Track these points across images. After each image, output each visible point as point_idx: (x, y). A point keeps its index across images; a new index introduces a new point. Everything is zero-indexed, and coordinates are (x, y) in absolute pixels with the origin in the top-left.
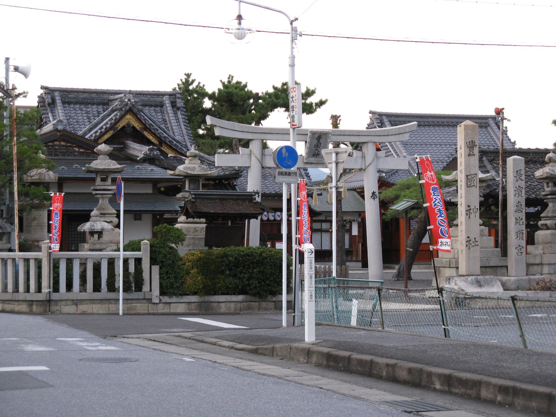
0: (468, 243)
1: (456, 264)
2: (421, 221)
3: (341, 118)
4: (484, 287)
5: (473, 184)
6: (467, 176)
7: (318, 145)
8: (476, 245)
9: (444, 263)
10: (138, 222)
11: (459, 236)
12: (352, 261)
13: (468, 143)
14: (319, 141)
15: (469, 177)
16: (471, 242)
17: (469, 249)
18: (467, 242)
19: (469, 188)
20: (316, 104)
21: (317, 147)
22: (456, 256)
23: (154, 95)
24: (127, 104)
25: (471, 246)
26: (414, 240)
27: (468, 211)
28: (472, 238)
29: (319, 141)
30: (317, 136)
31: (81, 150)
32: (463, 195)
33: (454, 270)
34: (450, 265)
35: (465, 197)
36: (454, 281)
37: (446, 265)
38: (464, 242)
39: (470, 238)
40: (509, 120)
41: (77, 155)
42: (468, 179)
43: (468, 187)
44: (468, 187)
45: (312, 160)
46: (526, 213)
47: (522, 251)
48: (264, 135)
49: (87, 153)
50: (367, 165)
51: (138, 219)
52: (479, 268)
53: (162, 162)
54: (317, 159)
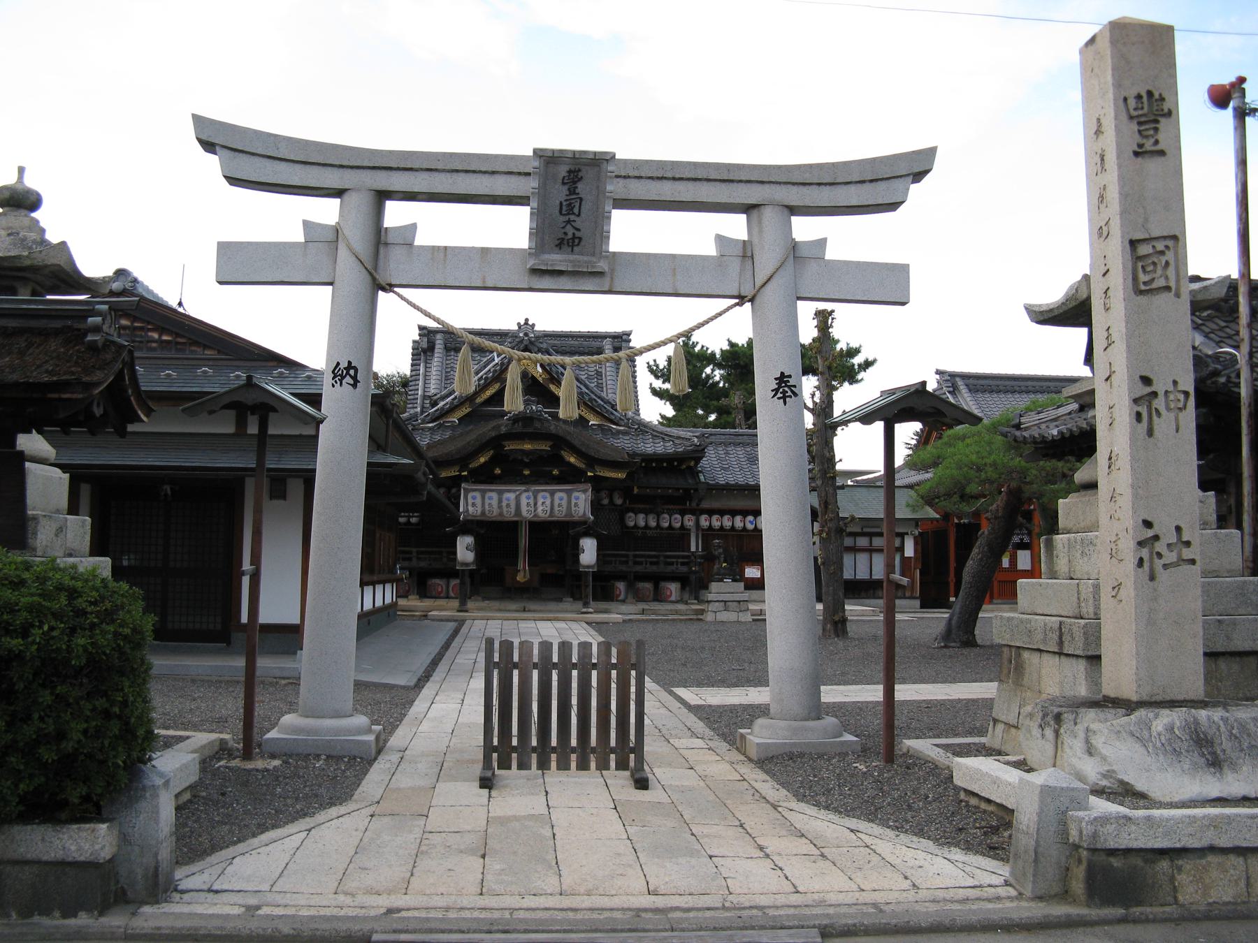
0: (1145, 553)
1: (1087, 644)
2: (996, 518)
3: (835, 315)
4: (1234, 767)
5: (1161, 283)
6: (1133, 244)
7: (570, 207)
8: (1182, 561)
9: (1039, 636)
11: (1104, 520)
12: (905, 597)
13: (1132, 103)
14: (572, 191)
15: (1144, 250)
16: (1160, 547)
17: (1152, 578)
18: (1141, 544)
19: (1143, 300)
20: (859, 365)
22: (1088, 609)
23: (589, 337)
24: (522, 341)
25: (1158, 563)
26: (981, 559)
29: (572, 191)
30: (563, 171)
31: (165, 338)
33: (1081, 665)
34: (1061, 643)
35: (1130, 336)
36: (1080, 729)
37: (1044, 641)
38: (1127, 546)
41: (154, 349)
45: (558, 259)
46: (617, 769)
48: (383, 174)
49: (177, 343)
50: (759, 281)
52: (1201, 659)
53: (546, 425)
54: (572, 257)
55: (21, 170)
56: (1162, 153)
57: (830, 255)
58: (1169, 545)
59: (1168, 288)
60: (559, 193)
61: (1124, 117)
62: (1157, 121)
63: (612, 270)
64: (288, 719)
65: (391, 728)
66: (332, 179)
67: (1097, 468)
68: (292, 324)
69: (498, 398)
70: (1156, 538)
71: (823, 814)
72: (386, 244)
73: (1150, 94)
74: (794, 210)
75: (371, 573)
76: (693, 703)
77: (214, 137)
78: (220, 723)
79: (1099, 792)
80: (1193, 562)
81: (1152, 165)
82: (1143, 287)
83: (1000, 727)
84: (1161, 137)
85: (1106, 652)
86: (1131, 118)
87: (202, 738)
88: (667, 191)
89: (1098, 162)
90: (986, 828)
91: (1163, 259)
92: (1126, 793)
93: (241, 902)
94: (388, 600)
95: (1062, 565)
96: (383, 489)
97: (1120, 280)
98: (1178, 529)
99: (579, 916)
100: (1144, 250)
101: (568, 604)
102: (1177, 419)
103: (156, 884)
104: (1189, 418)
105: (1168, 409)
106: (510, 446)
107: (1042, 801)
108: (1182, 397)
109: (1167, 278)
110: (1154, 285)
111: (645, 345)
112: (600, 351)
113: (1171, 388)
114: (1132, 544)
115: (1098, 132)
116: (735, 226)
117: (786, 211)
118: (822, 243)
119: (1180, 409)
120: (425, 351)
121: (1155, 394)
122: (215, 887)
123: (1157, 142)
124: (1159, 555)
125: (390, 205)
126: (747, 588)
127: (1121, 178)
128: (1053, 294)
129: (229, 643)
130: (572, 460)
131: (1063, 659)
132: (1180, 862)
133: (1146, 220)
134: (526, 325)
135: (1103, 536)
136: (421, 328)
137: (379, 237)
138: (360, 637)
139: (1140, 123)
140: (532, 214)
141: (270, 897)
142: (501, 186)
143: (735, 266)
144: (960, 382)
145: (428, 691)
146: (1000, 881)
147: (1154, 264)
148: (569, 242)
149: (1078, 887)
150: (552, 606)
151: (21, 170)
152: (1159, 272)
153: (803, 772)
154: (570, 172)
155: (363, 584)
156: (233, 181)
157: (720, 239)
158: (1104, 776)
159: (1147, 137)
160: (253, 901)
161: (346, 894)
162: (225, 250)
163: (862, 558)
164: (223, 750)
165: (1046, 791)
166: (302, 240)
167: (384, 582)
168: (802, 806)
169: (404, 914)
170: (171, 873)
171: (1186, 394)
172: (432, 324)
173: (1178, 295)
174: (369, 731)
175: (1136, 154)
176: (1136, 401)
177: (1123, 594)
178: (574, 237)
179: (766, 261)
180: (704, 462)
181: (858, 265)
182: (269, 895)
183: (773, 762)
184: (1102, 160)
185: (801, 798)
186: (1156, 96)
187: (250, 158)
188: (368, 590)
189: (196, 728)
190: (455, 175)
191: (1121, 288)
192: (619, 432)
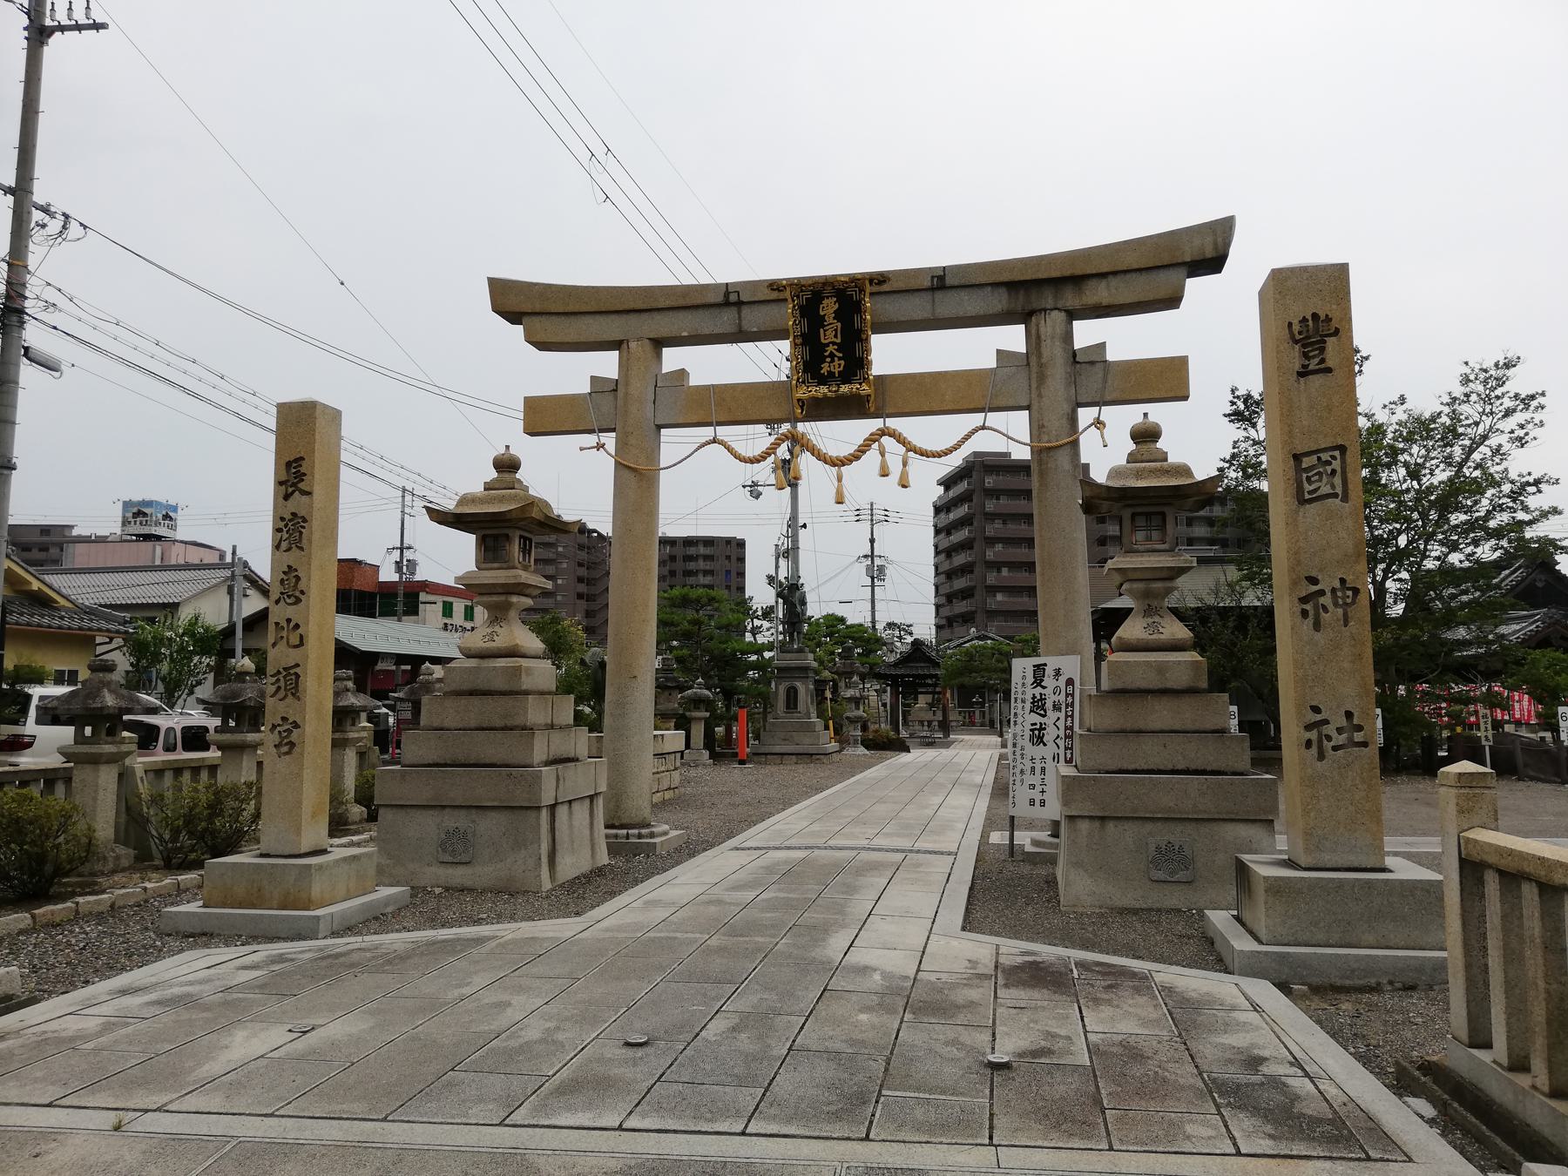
0: (1313, 735)
5: (1326, 490)
6: (1297, 458)
13: (1296, 328)
15: (1307, 462)
16: (1330, 730)
42: (1299, 469)
55: (507, 447)
56: (1329, 370)
59: (1335, 495)
70: (1326, 722)
77: (517, 303)
91: (1329, 469)
105: (1336, 605)
109: (1333, 487)
111: (919, 445)
123: (1323, 361)
124: (1329, 738)
139: (1304, 346)
151: (507, 447)
156: (542, 346)
186: (1323, 317)
187: (536, 311)
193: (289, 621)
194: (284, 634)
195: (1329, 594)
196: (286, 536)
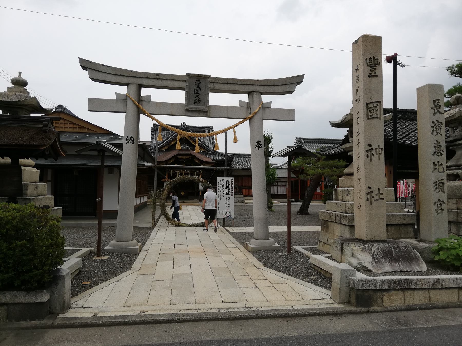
0: (369, 196)
6: (367, 104)
10: (112, 175)
11: (355, 186)
13: (368, 60)
14: (198, 87)
15: (370, 106)
16: (373, 195)
17: (371, 203)
21: (197, 93)
25: (373, 199)
27: (370, 151)
28: (375, 189)
29: (198, 87)
32: (362, 130)
33: (347, 228)
38: (363, 195)
39: (372, 190)
40: (403, 66)
42: (368, 108)
43: (380, 102)
44: (368, 119)
45: (195, 107)
47: (443, 207)
51: (111, 173)
55: (20, 73)
56: (377, 76)
57: (272, 107)
58: (376, 194)
59: (377, 118)
60: (194, 87)
61: (366, 65)
62: (376, 66)
63: (210, 110)
64: (113, 242)
65: (143, 244)
66: (125, 80)
67: (353, 168)
68: (115, 123)
69: (175, 144)
70: (372, 192)
71: (272, 271)
72: (142, 101)
73: (374, 58)
74: (262, 93)
75: (139, 193)
76: (231, 232)
77: (86, 65)
78: (90, 245)
79: (358, 269)
80: (383, 199)
81: (374, 80)
82: (370, 117)
83: (321, 244)
84: (376, 71)
85: (356, 223)
86: (368, 65)
87: (84, 250)
88: (225, 87)
89: (356, 79)
90: (322, 277)
91: (376, 109)
92: (366, 270)
93: (92, 311)
94: (145, 201)
95: (340, 197)
96: (143, 173)
97: (363, 115)
98: (379, 189)
99: (201, 311)
100: (370, 106)
101: (195, 200)
102: (379, 157)
103: (64, 307)
104: (383, 156)
105: (377, 154)
106: (179, 157)
107: (342, 274)
108: (380, 150)
109: (377, 114)
110: (373, 117)
112: (204, 132)
113: (377, 147)
114: (365, 194)
115: (357, 70)
116: (245, 98)
117: (260, 94)
118: (270, 103)
119: (380, 154)
120: (155, 131)
121: (372, 149)
122: (84, 306)
123: (375, 73)
124: (373, 197)
125: (143, 89)
126: (244, 196)
127: (364, 84)
128: (338, 119)
129: (96, 216)
130: (197, 162)
131: (341, 225)
132: (384, 293)
133: (371, 97)
134: (184, 124)
135: (356, 189)
136: (154, 124)
137: (140, 98)
138: (135, 213)
139: (370, 67)
140: (186, 93)
141: (102, 309)
142: (177, 84)
143: (245, 109)
144: (302, 141)
145: (155, 229)
146: (328, 297)
147: (373, 110)
148: (198, 102)
149: (353, 300)
150: (191, 201)
151: (20, 73)
152: (375, 112)
153: (266, 256)
154: (197, 81)
155: (136, 197)
156: (93, 79)
157: (240, 102)
158: (358, 264)
159: (372, 71)
160: (96, 311)
161: (127, 306)
162: (91, 101)
163: (275, 188)
164: (91, 253)
165: (343, 271)
166: (116, 99)
167: (143, 196)
168: (265, 268)
169: (146, 313)
170: (70, 301)
171: (382, 149)
172: (156, 123)
173: (380, 119)
174: (137, 245)
175: (369, 76)
176: (367, 151)
177: (361, 208)
178: (198, 100)
179: (255, 108)
180: (233, 162)
181: (280, 109)
182: (102, 308)
183: (255, 252)
184: (358, 78)
185: (265, 265)
188: (139, 199)
189: (83, 246)
190: (163, 80)
191: (363, 117)
192: (209, 154)
193: (438, 162)
194: (437, 167)
195: (374, 150)
196: (435, 129)
